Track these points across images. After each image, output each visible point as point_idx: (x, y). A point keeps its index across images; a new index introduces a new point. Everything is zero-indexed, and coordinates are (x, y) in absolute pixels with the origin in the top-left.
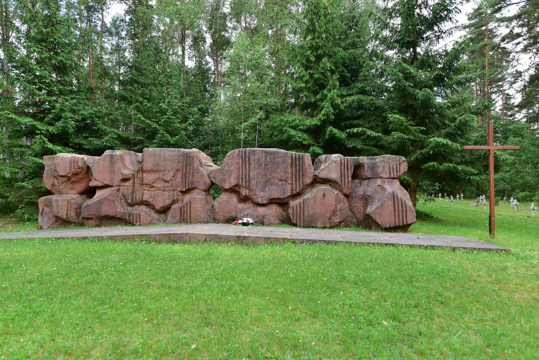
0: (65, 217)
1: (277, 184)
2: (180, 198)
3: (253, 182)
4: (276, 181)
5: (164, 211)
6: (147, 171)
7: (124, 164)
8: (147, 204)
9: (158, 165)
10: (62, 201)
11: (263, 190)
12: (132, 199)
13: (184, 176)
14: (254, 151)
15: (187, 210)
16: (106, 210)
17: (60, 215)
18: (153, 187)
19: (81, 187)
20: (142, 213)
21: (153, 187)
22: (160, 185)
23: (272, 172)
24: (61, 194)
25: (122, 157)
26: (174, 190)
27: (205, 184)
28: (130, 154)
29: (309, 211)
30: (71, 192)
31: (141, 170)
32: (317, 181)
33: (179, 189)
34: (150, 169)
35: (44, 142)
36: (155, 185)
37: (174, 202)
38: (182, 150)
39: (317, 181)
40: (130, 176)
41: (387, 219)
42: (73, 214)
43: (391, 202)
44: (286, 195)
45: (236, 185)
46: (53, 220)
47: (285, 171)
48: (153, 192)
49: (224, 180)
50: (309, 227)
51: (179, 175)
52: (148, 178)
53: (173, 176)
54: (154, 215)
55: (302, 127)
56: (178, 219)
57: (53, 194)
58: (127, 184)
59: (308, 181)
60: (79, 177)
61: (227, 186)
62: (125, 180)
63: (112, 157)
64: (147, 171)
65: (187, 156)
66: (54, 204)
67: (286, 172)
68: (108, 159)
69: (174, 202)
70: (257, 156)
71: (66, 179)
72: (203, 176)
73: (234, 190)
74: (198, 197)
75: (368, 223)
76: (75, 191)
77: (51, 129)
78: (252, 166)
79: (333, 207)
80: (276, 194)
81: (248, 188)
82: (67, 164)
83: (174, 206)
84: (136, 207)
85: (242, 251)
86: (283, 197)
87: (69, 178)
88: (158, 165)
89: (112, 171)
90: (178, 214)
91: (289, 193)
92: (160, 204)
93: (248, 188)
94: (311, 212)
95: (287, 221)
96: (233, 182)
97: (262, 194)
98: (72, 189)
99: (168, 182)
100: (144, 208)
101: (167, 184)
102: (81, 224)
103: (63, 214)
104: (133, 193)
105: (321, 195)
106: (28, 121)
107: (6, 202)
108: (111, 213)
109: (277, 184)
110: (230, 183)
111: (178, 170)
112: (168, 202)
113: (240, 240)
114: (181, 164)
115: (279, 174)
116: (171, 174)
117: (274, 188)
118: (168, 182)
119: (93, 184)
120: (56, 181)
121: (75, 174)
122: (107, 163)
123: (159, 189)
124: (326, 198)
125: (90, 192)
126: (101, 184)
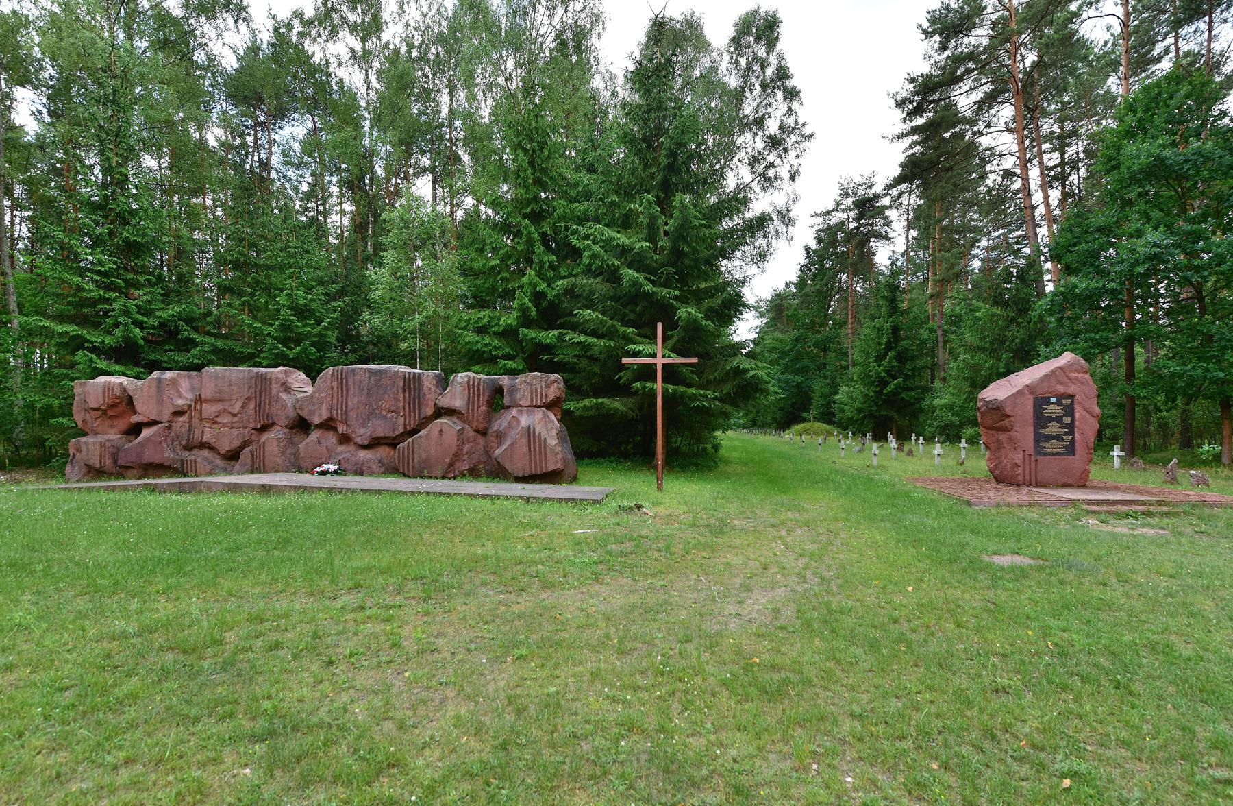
0: (98, 466)
1: (385, 417)
2: (254, 438)
3: (352, 414)
4: (384, 413)
5: (233, 456)
6: (207, 401)
7: (178, 391)
8: (211, 448)
9: (220, 391)
10: (94, 443)
11: (364, 425)
12: (188, 440)
13: (258, 407)
14: (353, 370)
15: (1144, 503)
16: (150, 456)
17: (91, 462)
18: (216, 423)
19: (122, 424)
20: (199, 460)
21: (216, 423)
22: (225, 420)
23: (377, 401)
24: (96, 434)
25: (174, 382)
26: (245, 428)
27: (287, 418)
28: (189, 377)
29: (421, 454)
30: (110, 431)
31: (199, 399)
32: (440, 412)
33: (252, 425)
34: (210, 397)
35: (91, 360)
36: (218, 420)
37: (245, 444)
38: (255, 370)
39: (440, 412)
40: (185, 408)
41: (520, 465)
42: (108, 462)
43: (524, 441)
44: (397, 433)
45: (331, 419)
46: (84, 470)
47: (393, 399)
48: (216, 430)
49: (312, 413)
50: (431, 477)
51: (252, 405)
52: (210, 410)
53: (243, 407)
54: (219, 462)
55: (495, 329)
56: (248, 467)
57: (86, 434)
58: (181, 419)
59: (429, 411)
60: (120, 409)
61: (317, 421)
62: (178, 413)
63: (159, 380)
64: (207, 401)
65: (263, 379)
66: (84, 448)
67: (397, 400)
68: (154, 384)
69: (245, 444)
70: (358, 377)
71: (100, 413)
72: (285, 407)
73: (328, 425)
74: (274, 437)
75: (499, 473)
76: (115, 430)
77: (108, 340)
78: (351, 392)
79: (454, 449)
80: (381, 430)
81: (345, 422)
82: (100, 391)
83: (247, 450)
84: (195, 452)
85: (265, 503)
86: (391, 434)
87: (104, 412)
88: (220, 391)
89: (160, 402)
90: (249, 460)
91: (401, 430)
92: (225, 447)
93: (345, 422)
94: (424, 456)
95: (393, 470)
96: (325, 414)
97: (362, 431)
98: (112, 426)
99: (235, 415)
100: (206, 453)
101: (236, 419)
102: (121, 476)
103: (95, 462)
104: (190, 430)
105: (437, 432)
106: (70, 328)
107: (35, 447)
108: (157, 459)
109: (385, 417)
110: (320, 416)
111: (249, 399)
112: (236, 444)
113: (265, 489)
114: (252, 390)
115: (387, 402)
116: (239, 404)
117: (379, 422)
118: (235, 415)
119: (135, 419)
120: (88, 417)
121: (112, 406)
122: (153, 390)
123: (224, 426)
124: (444, 436)
125: (135, 430)
126: (146, 420)
